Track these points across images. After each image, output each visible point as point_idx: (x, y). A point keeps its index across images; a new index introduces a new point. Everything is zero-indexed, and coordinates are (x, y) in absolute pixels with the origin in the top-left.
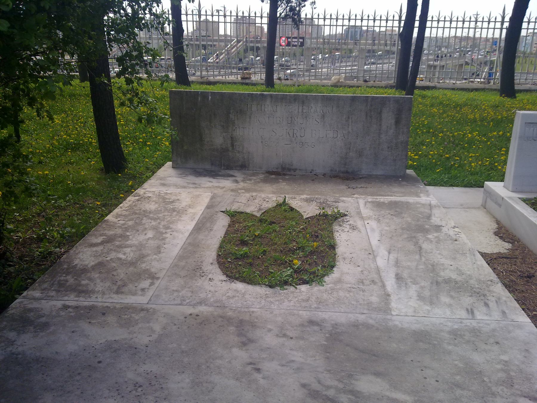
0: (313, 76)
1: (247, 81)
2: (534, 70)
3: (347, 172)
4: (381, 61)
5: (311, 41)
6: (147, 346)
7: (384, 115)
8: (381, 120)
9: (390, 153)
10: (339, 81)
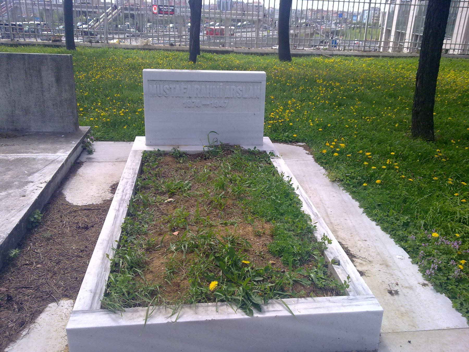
0: (183, 42)
1: (58, 43)
2: (371, 39)
3: (16, 130)
4: (245, 30)
5: (180, 10)
6: (409, 342)
7: (44, 73)
8: (41, 78)
9: (56, 110)
10: (147, 44)
